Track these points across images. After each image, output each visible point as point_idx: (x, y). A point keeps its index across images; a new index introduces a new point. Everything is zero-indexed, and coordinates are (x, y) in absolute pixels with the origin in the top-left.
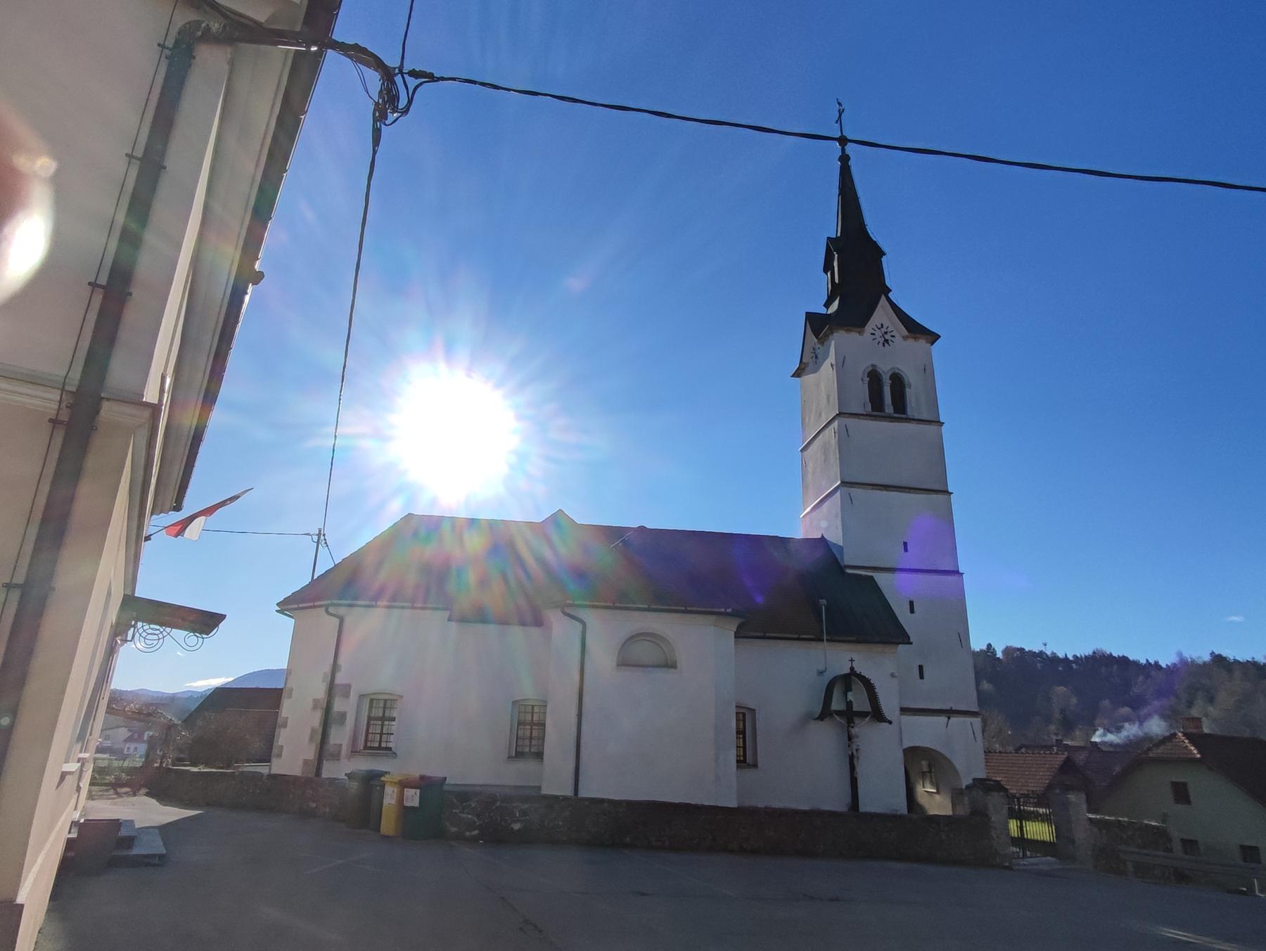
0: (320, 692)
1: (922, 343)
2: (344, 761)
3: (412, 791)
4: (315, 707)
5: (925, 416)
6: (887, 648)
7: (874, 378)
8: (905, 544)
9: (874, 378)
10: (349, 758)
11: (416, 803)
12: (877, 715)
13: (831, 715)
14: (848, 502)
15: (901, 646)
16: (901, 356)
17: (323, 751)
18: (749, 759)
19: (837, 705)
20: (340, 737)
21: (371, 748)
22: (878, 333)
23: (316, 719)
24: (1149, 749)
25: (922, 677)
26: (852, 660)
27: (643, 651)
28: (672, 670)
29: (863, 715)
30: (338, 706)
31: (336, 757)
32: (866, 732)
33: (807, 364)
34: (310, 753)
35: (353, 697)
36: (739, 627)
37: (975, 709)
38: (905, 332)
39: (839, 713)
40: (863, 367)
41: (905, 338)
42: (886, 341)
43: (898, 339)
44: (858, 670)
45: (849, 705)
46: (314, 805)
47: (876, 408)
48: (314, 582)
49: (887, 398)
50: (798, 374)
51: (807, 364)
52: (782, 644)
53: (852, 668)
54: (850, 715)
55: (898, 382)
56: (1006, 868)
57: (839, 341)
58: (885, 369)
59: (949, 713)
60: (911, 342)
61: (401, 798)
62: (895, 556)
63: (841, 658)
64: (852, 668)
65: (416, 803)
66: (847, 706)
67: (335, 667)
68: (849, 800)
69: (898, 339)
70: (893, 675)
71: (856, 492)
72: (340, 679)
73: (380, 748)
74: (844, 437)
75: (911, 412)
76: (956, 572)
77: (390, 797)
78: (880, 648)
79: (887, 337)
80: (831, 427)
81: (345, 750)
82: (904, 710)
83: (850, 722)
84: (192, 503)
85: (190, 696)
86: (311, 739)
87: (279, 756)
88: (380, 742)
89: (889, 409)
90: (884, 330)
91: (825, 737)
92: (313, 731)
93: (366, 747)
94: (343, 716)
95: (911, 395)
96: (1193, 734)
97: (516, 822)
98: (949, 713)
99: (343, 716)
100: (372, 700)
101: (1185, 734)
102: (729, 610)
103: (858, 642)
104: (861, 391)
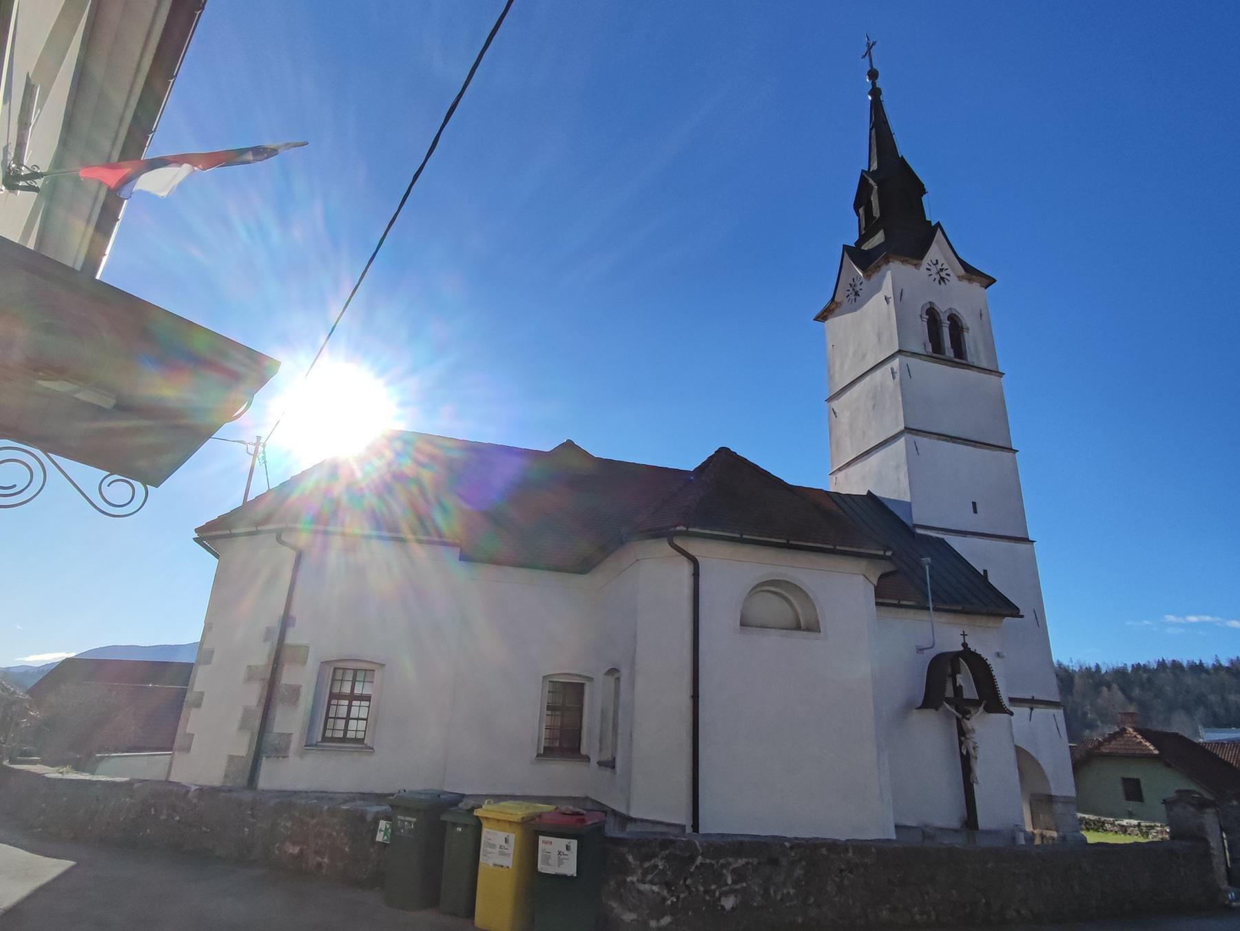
0: (261, 657)
3: (560, 843)
4: (250, 678)
5: (984, 365)
6: (991, 622)
7: (932, 315)
8: (974, 504)
9: (932, 315)
10: (301, 756)
11: (570, 868)
12: (991, 702)
14: (913, 455)
15: (1007, 619)
16: (960, 298)
17: (264, 744)
20: (290, 722)
21: (333, 740)
22: (934, 270)
23: (253, 696)
24: (1100, 744)
26: (964, 635)
27: (770, 607)
29: (975, 703)
30: (288, 677)
31: (281, 752)
32: (983, 725)
33: (839, 305)
34: (242, 747)
35: (312, 665)
36: (882, 577)
37: (1056, 698)
40: (918, 307)
42: (942, 279)
43: (953, 279)
44: (973, 646)
46: (295, 850)
48: (247, 505)
49: (944, 338)
50: (816, 319)
51: (839, 305)
53: (965, 645)
54: (963, 707)
57: (891, 276)
58: (942, 308)
60: (965, 283)
61: (529, 853)
62: (967, 521)
63: (949, 633)
64: (965, 645)
65: (570, 868)
66: (956, 689)
67: (286, 621)
68: (964, 812)
71: (923, 441)
72: (290, 639)
73: (344, 739)
74: (905, 379)
75: (971, 358)
76: (1026, 540)
77: (498, 850)
79: (943, 274)
80: (888, 367)
82: (1012, 700)
83: (965, 714)
84: (147, 155)
85: (27, 672)
86: (243, 726)
87: (187, 749)
88: (346, 730)
89: (949, 353)
90: (939, 266)
91: (930, 731)
92: (247, 713)
93: (324, 739)
94: (295, 692)
95: (968, 338)
96: (1157, 733)
97: (726, 894)
99: (295, 692)
100: (335, 669)
101: (1136, 730)
102: (889, 553)
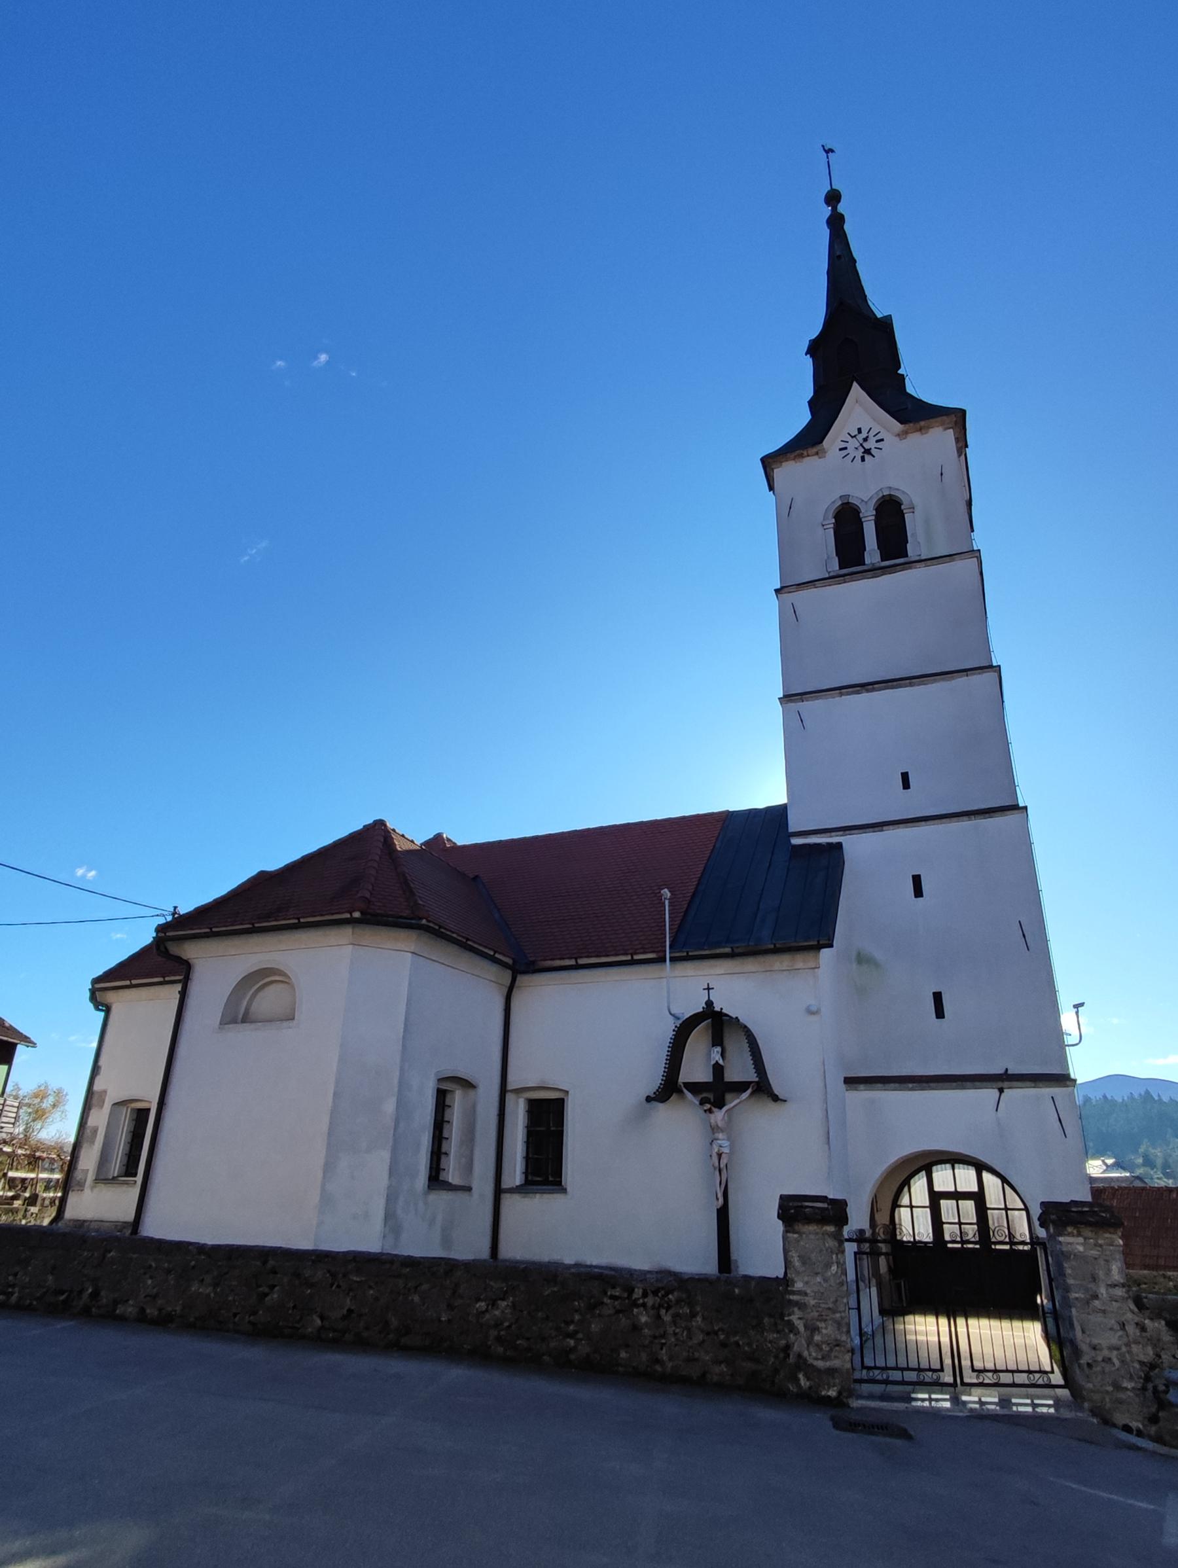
1: (941, 437)
2: (87, 1191)
6: (801, 961)
13: (680, 1092)
18: (452, 1175)
19: (696, 1069)
22: (853, 443)
25: (940, 1014)
28: (290, 1023)
32: (756, 1123)
38: (897, 426)
39: (694, 1088)
40: (828, 501)
41: (902, 435)
42: (868, 451)
45: (714, 1073)
47: (849, 555)
49: (869, 538)
52: (615, 974)
53: (709, 1003)
55: (891, 510)
56: (827, 1402)
59: (1003, 1080)
60: (915, 438)
63: (688, 986)
64: (709, 1003)
69: (890, 439)
70: (810, 1012)
71: (806, 706)
78: (781, 962)
79: (870, 445)
81: (91, 1177)
89: (872, 554)
98: (1003, 1080)
99: (95, 1131)
103: (732, 956)
104: (822, 545)
